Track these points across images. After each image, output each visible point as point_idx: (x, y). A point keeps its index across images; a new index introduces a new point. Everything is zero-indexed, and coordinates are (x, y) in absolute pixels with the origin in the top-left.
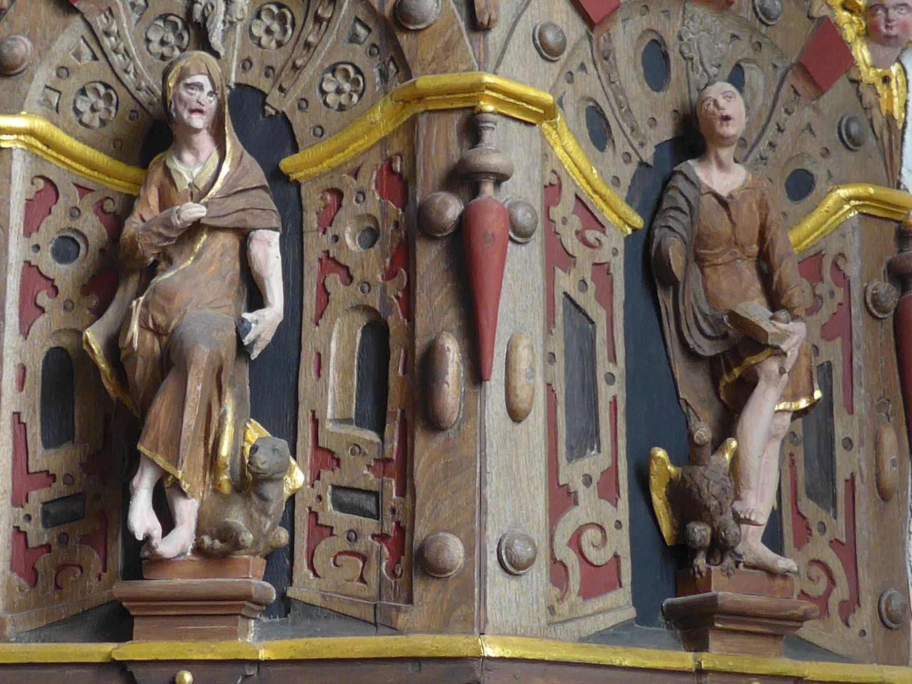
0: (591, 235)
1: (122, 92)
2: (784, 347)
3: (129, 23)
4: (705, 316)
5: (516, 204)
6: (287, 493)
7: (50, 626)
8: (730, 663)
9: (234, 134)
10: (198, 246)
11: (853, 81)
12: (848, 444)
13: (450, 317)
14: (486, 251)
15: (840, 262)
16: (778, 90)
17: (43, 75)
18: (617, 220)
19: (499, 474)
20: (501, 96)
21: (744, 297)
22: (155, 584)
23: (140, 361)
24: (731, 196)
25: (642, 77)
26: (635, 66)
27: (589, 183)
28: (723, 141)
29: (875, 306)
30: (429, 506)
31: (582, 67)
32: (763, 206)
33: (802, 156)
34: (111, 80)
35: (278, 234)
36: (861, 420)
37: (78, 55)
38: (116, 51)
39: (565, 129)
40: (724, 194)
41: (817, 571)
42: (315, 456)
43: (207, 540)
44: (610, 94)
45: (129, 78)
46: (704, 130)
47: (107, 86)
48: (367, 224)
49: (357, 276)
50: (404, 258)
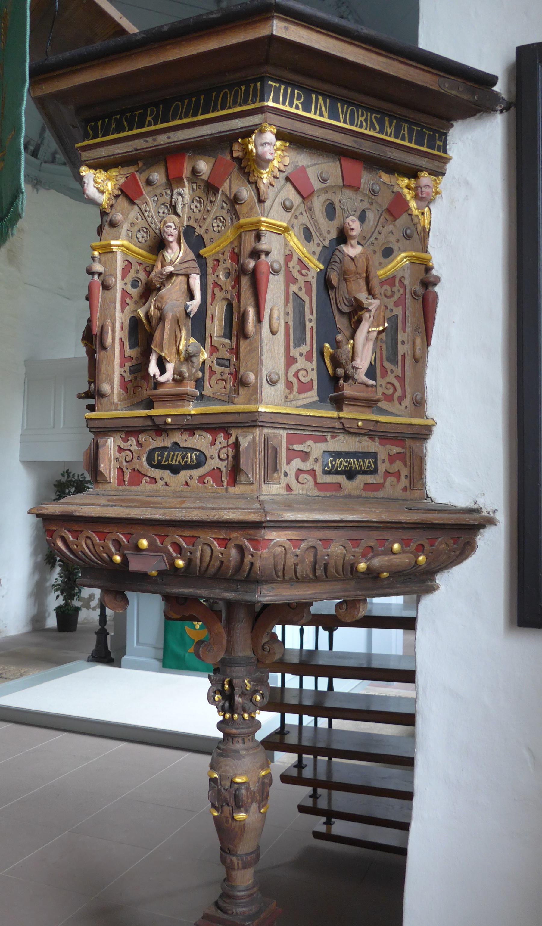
0: (304, 272)
1: (151, 230)
2: (370, 308)
3: (153, 207)
4: (346, 299)
5: (273, 262)
6: (201, 360)
7: (131, 405)
8: (350, 416)
9: (185, 243)
10: (173, 281)
11: (409, 215)
12: (403, 343)
13: (251, 301)
14: (262, 279)
15: (402, 280)
16: (380, 218)
17: (126, 226)
18: (314, 266)
19: (267, 352)
20: (267, 225)
21: (360, 291)
22: (160, 391)
23: (154, 319)
24: (355, 257)
25: (325, 216)
26: (322, 212)
27: (303, 254)
28: (353, 237)
29: (415, 295)
30: (244, 363)
31: (301, 213)
32: (367, 260)
33: (389, 242)
34: (147, 227)
35: (199, 276)
36: (408, 335)
37: (137, 219)
38: (149, 217)
39: (294, 235)
40: (353, 256)
41: (389, 386)
42: (211, 348)
43: (176, 376)
44: (312, 222)
45: (153, 226)
46: (346, 234)
47: (146, 229)
48: (227, 271)
49: (224, 288)
50: (237, 282)
